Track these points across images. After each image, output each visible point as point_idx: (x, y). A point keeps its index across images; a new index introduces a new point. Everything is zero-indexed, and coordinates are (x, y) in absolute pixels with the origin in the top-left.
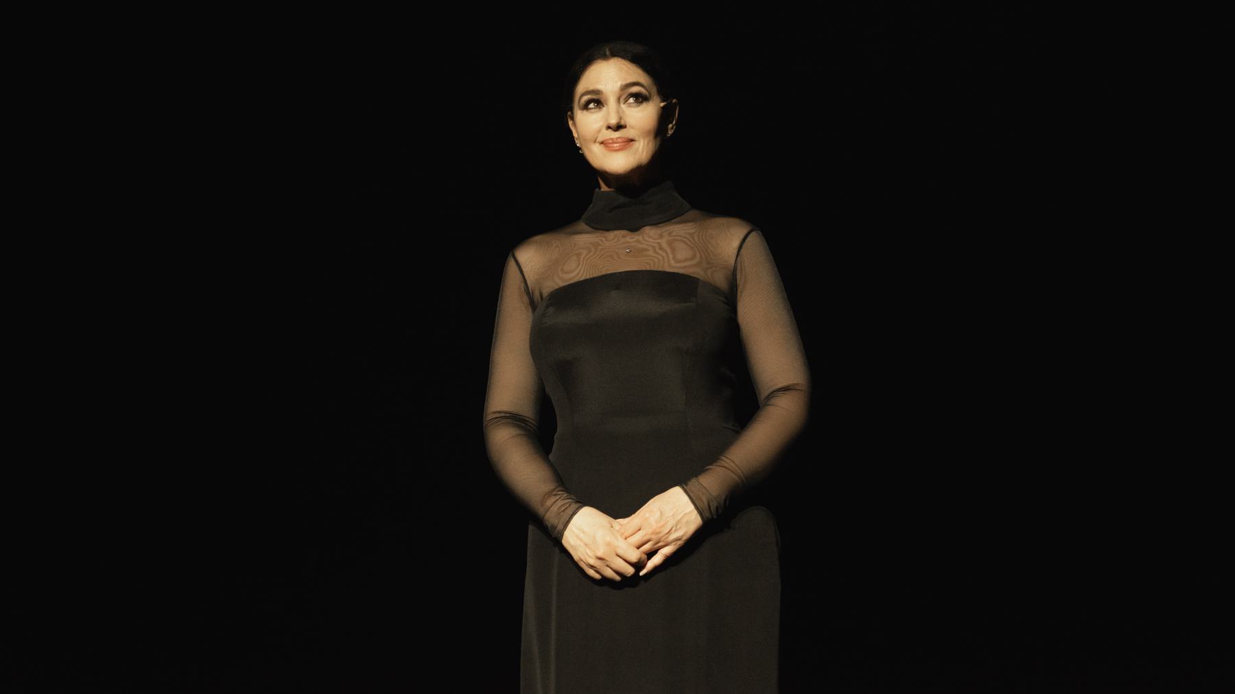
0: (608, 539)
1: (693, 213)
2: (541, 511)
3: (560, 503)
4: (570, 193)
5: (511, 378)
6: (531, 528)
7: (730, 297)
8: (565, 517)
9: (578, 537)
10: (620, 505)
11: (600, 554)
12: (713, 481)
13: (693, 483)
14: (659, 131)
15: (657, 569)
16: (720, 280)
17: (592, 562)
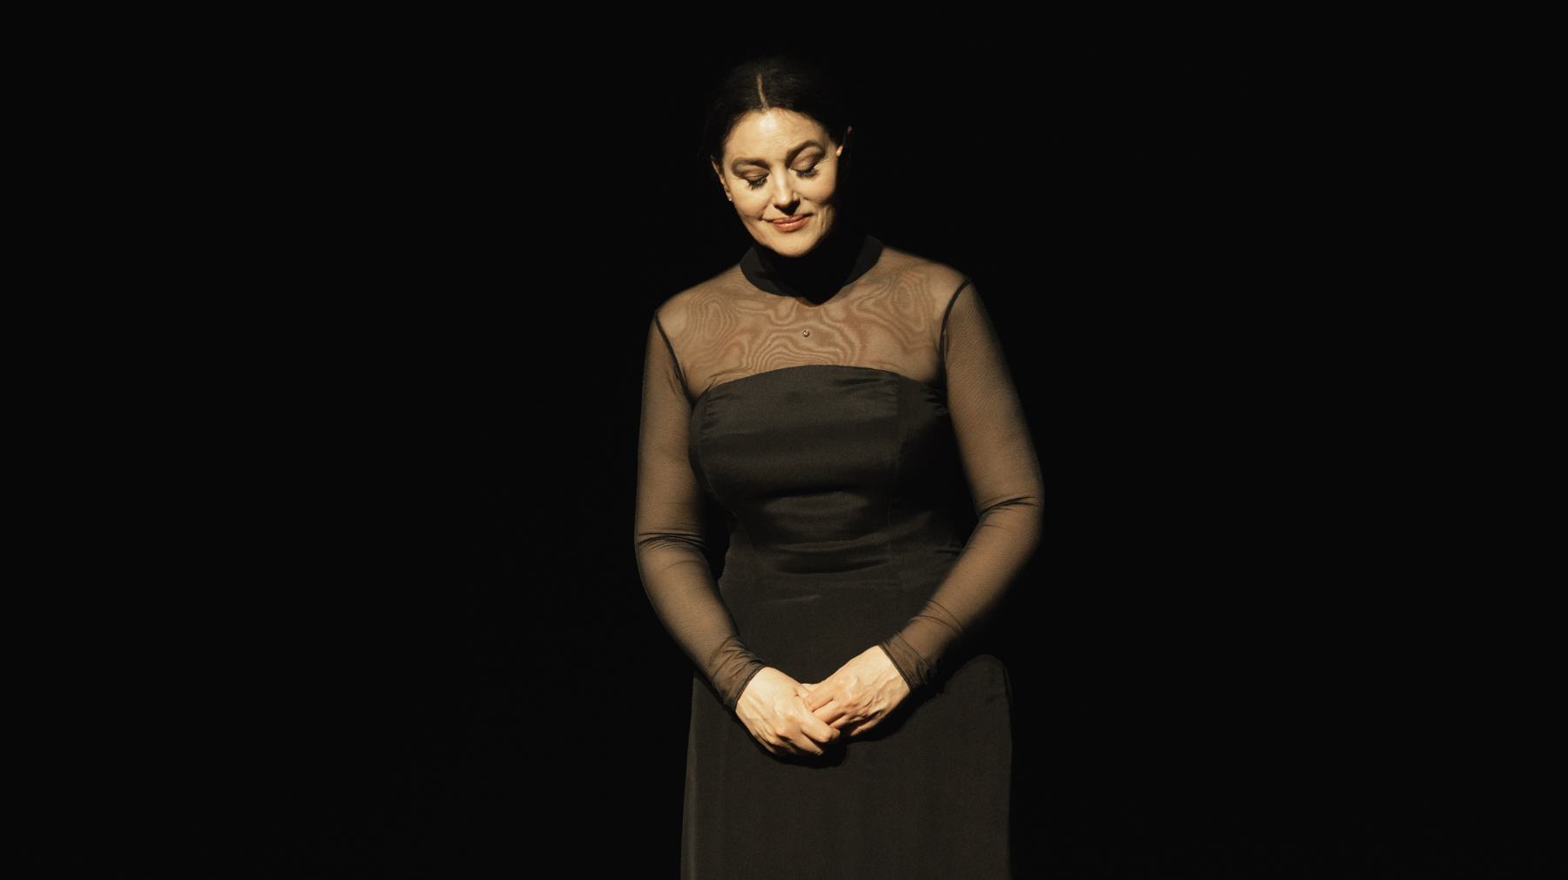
0: (791, 713)
1: (889, 259)
2: (711, 671)
3: (732, 664)
4: (716, 242)
5: (663, 488)
6: (695, 680)
7: (938, 385)
8: (738, 681)
9: (754, 707)
10: (810, 667)
11: (781, 731)
12: (923, 634)
13: (896, 640)
14: (835, 201)
15: (862, 733)
16: (916, 366)
17: (773, 740)
